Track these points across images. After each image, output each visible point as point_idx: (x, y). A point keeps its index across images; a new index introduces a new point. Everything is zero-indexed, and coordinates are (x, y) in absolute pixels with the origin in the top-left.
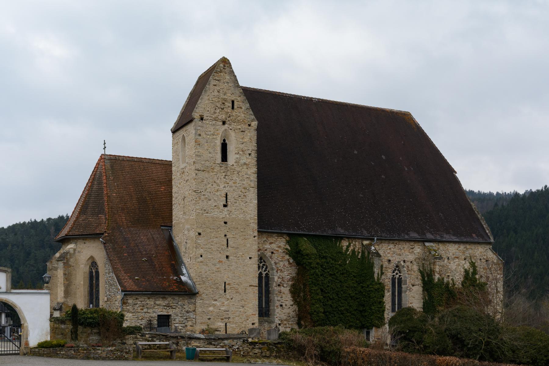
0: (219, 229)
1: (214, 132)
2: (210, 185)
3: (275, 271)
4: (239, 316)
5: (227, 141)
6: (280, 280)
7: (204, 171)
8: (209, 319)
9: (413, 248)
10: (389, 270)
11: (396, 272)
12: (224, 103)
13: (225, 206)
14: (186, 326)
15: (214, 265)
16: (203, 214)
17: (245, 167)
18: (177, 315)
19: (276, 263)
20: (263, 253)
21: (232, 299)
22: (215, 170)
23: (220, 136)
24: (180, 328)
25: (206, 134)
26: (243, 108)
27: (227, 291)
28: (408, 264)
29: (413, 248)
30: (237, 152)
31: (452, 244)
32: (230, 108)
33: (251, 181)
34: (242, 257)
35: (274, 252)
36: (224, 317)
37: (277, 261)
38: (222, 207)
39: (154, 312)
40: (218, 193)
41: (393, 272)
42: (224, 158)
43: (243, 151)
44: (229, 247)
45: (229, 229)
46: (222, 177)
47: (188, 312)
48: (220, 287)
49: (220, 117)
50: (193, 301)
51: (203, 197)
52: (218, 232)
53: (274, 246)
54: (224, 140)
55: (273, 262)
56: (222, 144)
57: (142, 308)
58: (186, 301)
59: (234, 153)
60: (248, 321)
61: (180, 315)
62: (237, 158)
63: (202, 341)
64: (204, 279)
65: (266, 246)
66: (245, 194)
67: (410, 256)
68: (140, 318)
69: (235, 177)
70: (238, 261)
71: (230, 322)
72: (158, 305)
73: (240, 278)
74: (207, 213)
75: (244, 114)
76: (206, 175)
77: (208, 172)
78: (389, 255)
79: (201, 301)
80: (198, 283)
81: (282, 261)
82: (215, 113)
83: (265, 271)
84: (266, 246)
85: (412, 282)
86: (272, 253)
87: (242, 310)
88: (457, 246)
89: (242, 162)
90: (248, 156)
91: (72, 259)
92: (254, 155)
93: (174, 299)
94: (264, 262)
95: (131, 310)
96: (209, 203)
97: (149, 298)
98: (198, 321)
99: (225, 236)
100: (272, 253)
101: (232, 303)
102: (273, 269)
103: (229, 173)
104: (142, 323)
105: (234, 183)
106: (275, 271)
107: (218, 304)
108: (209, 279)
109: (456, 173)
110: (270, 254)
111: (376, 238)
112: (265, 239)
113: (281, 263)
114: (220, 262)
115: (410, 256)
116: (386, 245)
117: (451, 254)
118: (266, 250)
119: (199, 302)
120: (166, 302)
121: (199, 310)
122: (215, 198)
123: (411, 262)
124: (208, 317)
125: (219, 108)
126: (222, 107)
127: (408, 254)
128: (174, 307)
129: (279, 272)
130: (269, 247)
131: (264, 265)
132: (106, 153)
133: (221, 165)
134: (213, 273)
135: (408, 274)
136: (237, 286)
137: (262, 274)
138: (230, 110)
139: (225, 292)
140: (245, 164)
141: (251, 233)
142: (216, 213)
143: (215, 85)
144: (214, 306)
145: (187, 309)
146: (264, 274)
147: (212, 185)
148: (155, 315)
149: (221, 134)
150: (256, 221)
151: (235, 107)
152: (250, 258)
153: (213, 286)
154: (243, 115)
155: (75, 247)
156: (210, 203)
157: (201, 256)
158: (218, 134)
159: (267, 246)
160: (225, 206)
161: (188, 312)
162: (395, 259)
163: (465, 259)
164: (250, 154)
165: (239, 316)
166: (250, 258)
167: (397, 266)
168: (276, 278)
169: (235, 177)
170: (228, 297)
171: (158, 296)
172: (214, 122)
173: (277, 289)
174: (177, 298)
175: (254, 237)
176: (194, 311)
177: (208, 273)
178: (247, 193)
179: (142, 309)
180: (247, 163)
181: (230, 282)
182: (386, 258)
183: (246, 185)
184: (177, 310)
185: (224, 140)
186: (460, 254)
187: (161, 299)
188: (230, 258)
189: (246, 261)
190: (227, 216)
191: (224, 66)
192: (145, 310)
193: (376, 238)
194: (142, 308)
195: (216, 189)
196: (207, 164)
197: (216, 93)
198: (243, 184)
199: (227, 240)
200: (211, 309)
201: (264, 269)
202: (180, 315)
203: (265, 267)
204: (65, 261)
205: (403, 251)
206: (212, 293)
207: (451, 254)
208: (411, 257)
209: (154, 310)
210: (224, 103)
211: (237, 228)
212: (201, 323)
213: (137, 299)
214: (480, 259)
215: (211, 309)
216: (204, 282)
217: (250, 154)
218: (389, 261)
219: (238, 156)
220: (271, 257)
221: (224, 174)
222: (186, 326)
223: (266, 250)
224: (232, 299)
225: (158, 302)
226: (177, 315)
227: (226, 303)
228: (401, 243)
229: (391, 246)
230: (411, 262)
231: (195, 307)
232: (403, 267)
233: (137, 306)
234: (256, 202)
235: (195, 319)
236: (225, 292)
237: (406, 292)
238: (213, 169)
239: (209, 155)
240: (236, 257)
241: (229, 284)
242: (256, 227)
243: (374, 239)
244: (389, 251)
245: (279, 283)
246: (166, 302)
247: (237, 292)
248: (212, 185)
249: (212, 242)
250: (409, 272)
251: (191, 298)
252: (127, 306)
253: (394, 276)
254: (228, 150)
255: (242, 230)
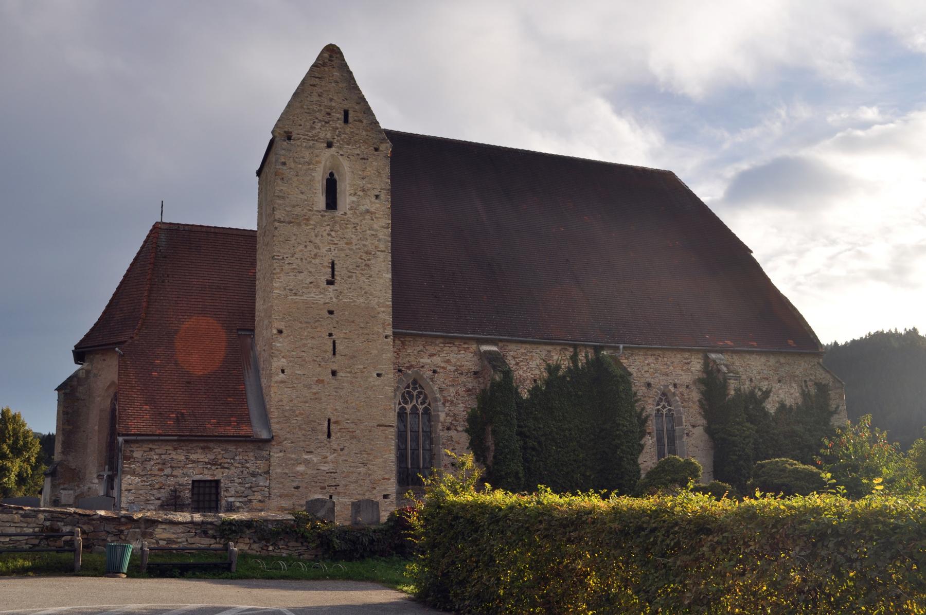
0: (316, 324)
1: (311, 159)
2: (301, 247)
3: (440, 404)
4: (356, 482)
5: (336, 176)
6: (449, 420)
7: (290, 223)
8: (297, 488)
9: (688, 363)
10: (650, 401)
11: (662, 404)
12: (329, 114)
13: (330, 283)
14: (250, 501)
15: (309, 387)
16: (286, 296)
17: (368, 217)
18: (232, 481)
19: (441, 390)
20: (416, 372)
21: (342, 450)
22: (312, 222)
23: (322, 165)
24: (238, 504)
25: (295, 162)
26: (365, 121)
27: (333, 434)
28: (682, 389)
29: (688, 363)
30: (352, 192)
31: (754, 356)
32: (341, 122)
33: (379, 240)
34: (362, 372)
35: (438, 370)
36: (326, 484)
37: (444, 386)
38: (324, 285)
39: (185, 475)
40: (317, 261)
41: (658, 405)
42: (332, 203)
43: (363, 191)
44: (337, 355)
45: (337, 322)
46: (325, 234)
47: (254, 475)
48: (319, 428)
49: (322, 135)
50: (264, 453)
51: (286, 267)
52: (316, 327)
53: (437, 360)
54: (331, 174)
55: (436, 388)
56: (328, 180)
57: (160, 466)
58: (252, 454)
59: (347, 193)
60: (375, 491)
61: (237, 481)
62: (353, 202)
63: (180, 529)
64: (286, 414)
65: (422, 360)
66: (368, 262)
67: (684, 377)
68: (157, 486)
69: (349, 233)
70: (354, 380)
71: (339, 494)
72: (194, 462)
73: (359, 411)
74: (295, 294)
75: (366, 131)
76: (295, 229)
77: (299, 225)
78: (647, 375)
79: (281, 454)
80: (276, 420)
81: (453, 385)
82: (312, 128)
83: (422, 404)
84: (422, 360)
85: (692, 420)
86: (435, 372)
87: (362, 470)
88: (763, 359)
89: (363, 208)
90: (373, 199)
91: (81, 388)
92: (386, 197)
93: (226, 450)
94: (421, 387)
95: (139, 470)
96: (299, 278)
97: (175, 449)
98: (275, 491)
99: (330, 335)
100: (435, 372)
101: (344, 458)
102: (436, 400)
103: (337, 227)
104: (159, 495)
105: (347, 244)
106: (440, 404)
107: (315, 459)
108: (297, 412)
109: (751, 252)
110: (431, 373)
111: (621, 346)
112: (421, 347)
113: (452, 389)
114: (320, 381)
115: (684, 377)
116: (642, 358)
117: (754, 372)
118: (423, 367)
119: (276, 455)
120: (211, 456)
121: (276, 470)
122: (311, 269)
123: (687, 387)
124: (295, 484)
125: (320, 121)
126: (327, 118)
127: (681, 372)
128: (226, 465)
129: (447, 404)
130: (429, 361)
131: (420, 393)
132: (165, 220)
133: (323, 213)
134: (306, 402)
135: (684, 407)
136: (352, 426)
137: (417, 409)
138: (340, 124)
139: (329, 436)
140: (368, 211)
141: (380, 331)
142: (313, 296)
143: (314, 86)
144: (307, 462)
145: (252, 469)
146: (421, 408)
147: (306, 247)
148: (187, 480)
149: (323, 163)
150: (390, 310)
151: (350, 120)
152: (379, 375)
153: (304, 426)
154: (364, 133)
155: (90, 368)
156: (300, 277)
157: (283, 371)
158: (318, 162)
159: (425, 360)
160: (330, 283)
161: (254, 475)
162: (659, 382)
163: (779, 381)
164: (377, 197)
165: (356, 482)
166: (379, 375)
167: (664, 394)
168: (442, 416)
169: (349, 233)
170: (335, 447)
171: (194, 445)
172: (311, 143)
173: (444, 434)
174: (232, 448)
175: (386, 337)
176: (268, 472)
177: (295, 402)
178: (373, 262)
179: (161, 470)
180: (372, 210)
181: (339, 419)
182: (643, 380)
183: (371, 248)
184: (233, 470)
185: (331, 174)
186: (771, 373)
187: (199, 451)
188: (341, 374)
189: (371, 379)
190: (334, 300)
191: (331, 56)
192: (167, 471)
193: (621, 346)
194: (160, 466)
195: (313, 253)
196: (297, 211)
197: (315, 98)
198: (364, 245)
199: (334, 343)
200: (301, 468)
201: (420, 401)
202: (237, 481)
203: (422, 397)
204: (67, 391)
205: (671, 368)
206: (303, 438)
207: (754, 372)
208: (686, 378)
209: (185, 471)
210: (329, 114)
211: (353, 322)
212: (280, 496)
213: (151, 449)
214: (805, 381)
215: (301, 468)
216: (288, 419)
217: (377, 197)
218: (649, 385)
219: (354, 199)
220: (432, 379)
221: (328, 228)
222: (250, 501)
223: (423, 367)
224: (342, 450)
225: (193, 457)
226: (232, 481)
227: (331, 457)
228: (667, 354)
229: (651, 360)
230: (687, 387)
231: (269, 466)
232: (674, 394)
233: (152, 463)
234: (389, 276)
235: (269, 487)
236: (329, 436)
237: (681, 437)
238: (308, 220)
239: (301, 196)
240: (350, 372)
241: (336, 422)
242: (389, 319)
243: (618, 347)
244: (646, 368)
245: (448, 425)
246: (211, 456)
247: (353, 438)
248: (306, 247)
249: (304, 345)
250: (685, 404)
251: (259, 448)
252: (129, 464)
253: (658, 410)
254: (338, 191)
255: (362, 325)
